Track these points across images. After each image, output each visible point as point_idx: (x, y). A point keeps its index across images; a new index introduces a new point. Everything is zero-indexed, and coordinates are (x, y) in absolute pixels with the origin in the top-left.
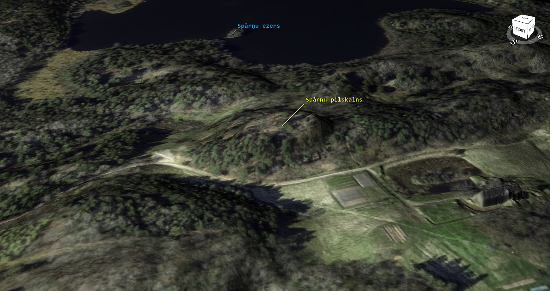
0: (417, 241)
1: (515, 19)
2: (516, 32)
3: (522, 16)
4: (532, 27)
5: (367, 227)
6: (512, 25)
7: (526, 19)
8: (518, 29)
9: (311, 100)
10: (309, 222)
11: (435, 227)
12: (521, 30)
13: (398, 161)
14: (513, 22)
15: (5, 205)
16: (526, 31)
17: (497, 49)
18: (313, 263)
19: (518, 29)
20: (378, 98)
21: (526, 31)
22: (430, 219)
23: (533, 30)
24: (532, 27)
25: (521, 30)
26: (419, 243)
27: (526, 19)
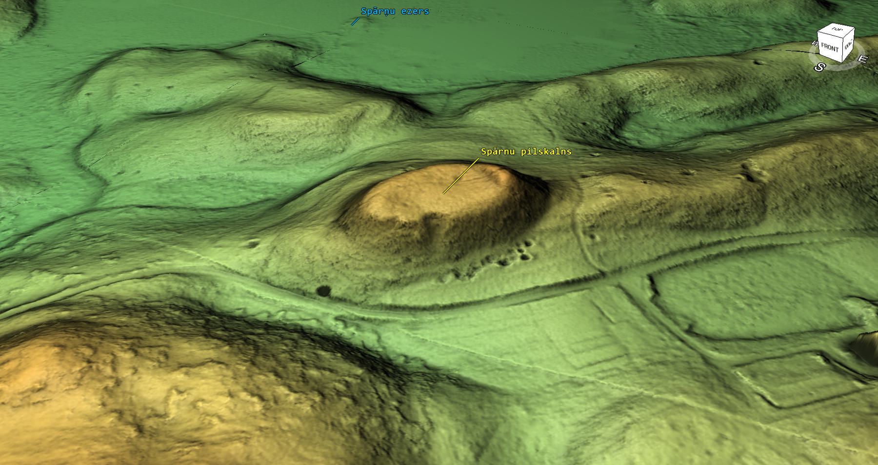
0: (745, 450)
1: (822, 30)
2: (824, 51)
3: (833, 25)
4: (850, 44)
5: (629, 416)
6: (817, 41)
7: (839, 30)
8: (827, 47)
9: (490, 152)
10: (500, 403)
11: (782, 413)
12: (832, 48)
13: (378, 268)
14: (819, 35)
15: (734, 190)
16: (840, 50)
17: (247, 289)
18: (400, 388)
19: (827, 47)
20: (634, 139)
21: (840, 50)
22: (769, 398)
23: (850, 48)
24: (850, 44)
25: (832, 48)
26: (751, 455)
27: (839, 30)
